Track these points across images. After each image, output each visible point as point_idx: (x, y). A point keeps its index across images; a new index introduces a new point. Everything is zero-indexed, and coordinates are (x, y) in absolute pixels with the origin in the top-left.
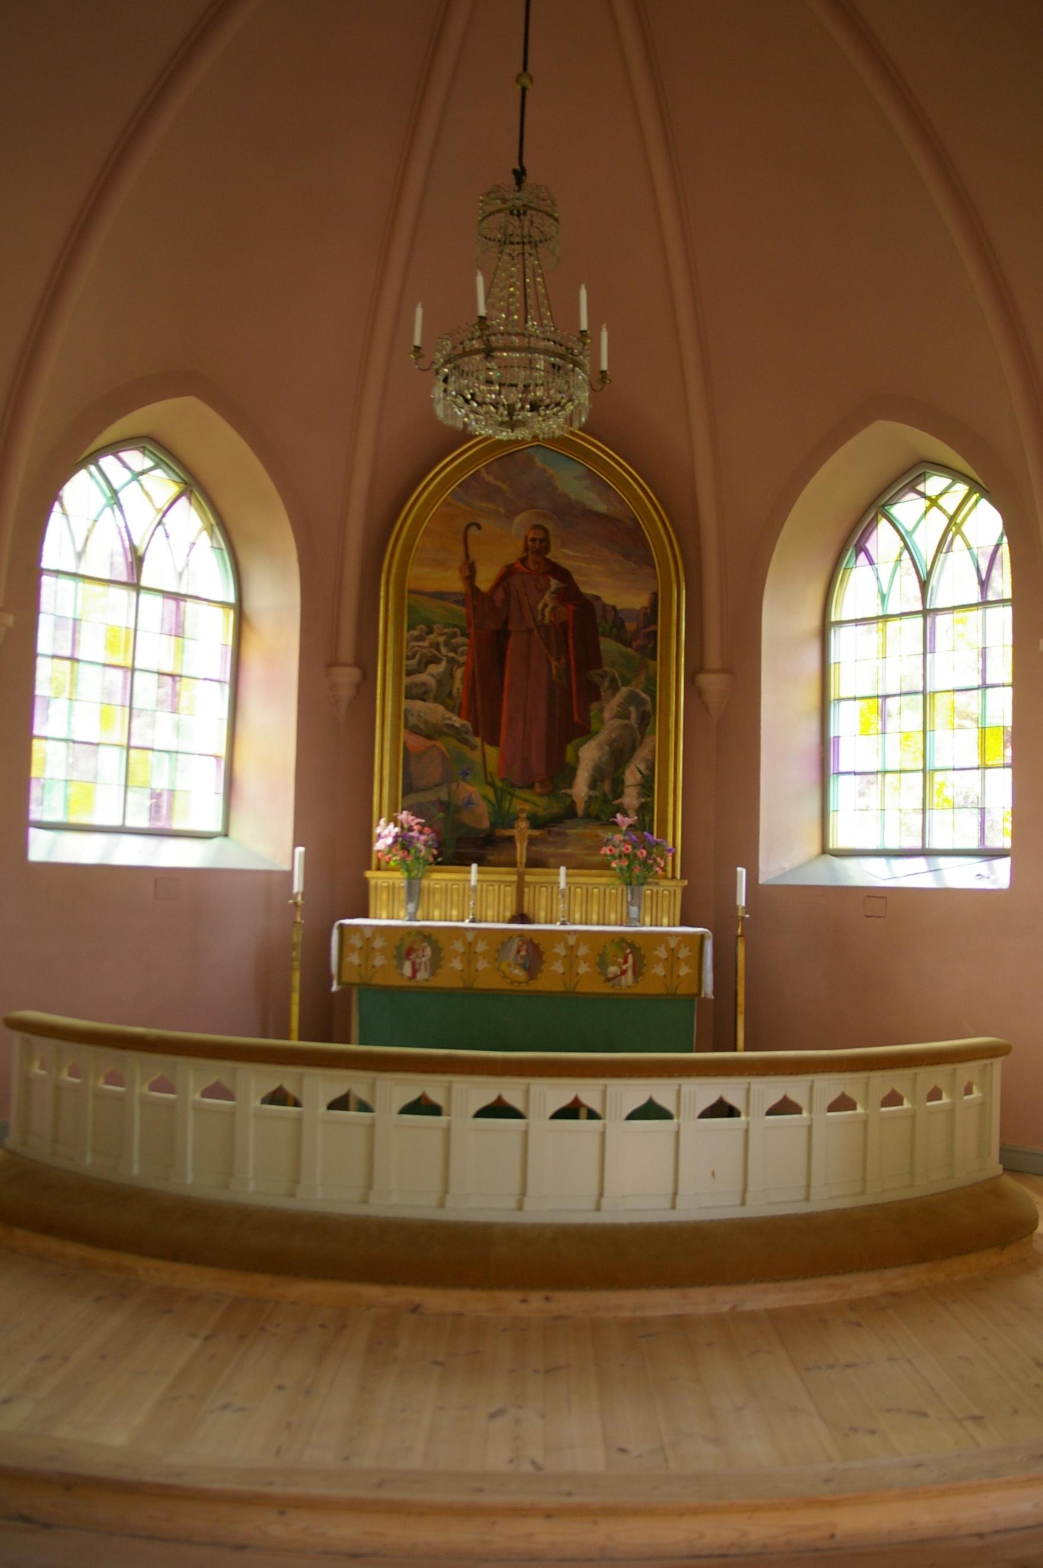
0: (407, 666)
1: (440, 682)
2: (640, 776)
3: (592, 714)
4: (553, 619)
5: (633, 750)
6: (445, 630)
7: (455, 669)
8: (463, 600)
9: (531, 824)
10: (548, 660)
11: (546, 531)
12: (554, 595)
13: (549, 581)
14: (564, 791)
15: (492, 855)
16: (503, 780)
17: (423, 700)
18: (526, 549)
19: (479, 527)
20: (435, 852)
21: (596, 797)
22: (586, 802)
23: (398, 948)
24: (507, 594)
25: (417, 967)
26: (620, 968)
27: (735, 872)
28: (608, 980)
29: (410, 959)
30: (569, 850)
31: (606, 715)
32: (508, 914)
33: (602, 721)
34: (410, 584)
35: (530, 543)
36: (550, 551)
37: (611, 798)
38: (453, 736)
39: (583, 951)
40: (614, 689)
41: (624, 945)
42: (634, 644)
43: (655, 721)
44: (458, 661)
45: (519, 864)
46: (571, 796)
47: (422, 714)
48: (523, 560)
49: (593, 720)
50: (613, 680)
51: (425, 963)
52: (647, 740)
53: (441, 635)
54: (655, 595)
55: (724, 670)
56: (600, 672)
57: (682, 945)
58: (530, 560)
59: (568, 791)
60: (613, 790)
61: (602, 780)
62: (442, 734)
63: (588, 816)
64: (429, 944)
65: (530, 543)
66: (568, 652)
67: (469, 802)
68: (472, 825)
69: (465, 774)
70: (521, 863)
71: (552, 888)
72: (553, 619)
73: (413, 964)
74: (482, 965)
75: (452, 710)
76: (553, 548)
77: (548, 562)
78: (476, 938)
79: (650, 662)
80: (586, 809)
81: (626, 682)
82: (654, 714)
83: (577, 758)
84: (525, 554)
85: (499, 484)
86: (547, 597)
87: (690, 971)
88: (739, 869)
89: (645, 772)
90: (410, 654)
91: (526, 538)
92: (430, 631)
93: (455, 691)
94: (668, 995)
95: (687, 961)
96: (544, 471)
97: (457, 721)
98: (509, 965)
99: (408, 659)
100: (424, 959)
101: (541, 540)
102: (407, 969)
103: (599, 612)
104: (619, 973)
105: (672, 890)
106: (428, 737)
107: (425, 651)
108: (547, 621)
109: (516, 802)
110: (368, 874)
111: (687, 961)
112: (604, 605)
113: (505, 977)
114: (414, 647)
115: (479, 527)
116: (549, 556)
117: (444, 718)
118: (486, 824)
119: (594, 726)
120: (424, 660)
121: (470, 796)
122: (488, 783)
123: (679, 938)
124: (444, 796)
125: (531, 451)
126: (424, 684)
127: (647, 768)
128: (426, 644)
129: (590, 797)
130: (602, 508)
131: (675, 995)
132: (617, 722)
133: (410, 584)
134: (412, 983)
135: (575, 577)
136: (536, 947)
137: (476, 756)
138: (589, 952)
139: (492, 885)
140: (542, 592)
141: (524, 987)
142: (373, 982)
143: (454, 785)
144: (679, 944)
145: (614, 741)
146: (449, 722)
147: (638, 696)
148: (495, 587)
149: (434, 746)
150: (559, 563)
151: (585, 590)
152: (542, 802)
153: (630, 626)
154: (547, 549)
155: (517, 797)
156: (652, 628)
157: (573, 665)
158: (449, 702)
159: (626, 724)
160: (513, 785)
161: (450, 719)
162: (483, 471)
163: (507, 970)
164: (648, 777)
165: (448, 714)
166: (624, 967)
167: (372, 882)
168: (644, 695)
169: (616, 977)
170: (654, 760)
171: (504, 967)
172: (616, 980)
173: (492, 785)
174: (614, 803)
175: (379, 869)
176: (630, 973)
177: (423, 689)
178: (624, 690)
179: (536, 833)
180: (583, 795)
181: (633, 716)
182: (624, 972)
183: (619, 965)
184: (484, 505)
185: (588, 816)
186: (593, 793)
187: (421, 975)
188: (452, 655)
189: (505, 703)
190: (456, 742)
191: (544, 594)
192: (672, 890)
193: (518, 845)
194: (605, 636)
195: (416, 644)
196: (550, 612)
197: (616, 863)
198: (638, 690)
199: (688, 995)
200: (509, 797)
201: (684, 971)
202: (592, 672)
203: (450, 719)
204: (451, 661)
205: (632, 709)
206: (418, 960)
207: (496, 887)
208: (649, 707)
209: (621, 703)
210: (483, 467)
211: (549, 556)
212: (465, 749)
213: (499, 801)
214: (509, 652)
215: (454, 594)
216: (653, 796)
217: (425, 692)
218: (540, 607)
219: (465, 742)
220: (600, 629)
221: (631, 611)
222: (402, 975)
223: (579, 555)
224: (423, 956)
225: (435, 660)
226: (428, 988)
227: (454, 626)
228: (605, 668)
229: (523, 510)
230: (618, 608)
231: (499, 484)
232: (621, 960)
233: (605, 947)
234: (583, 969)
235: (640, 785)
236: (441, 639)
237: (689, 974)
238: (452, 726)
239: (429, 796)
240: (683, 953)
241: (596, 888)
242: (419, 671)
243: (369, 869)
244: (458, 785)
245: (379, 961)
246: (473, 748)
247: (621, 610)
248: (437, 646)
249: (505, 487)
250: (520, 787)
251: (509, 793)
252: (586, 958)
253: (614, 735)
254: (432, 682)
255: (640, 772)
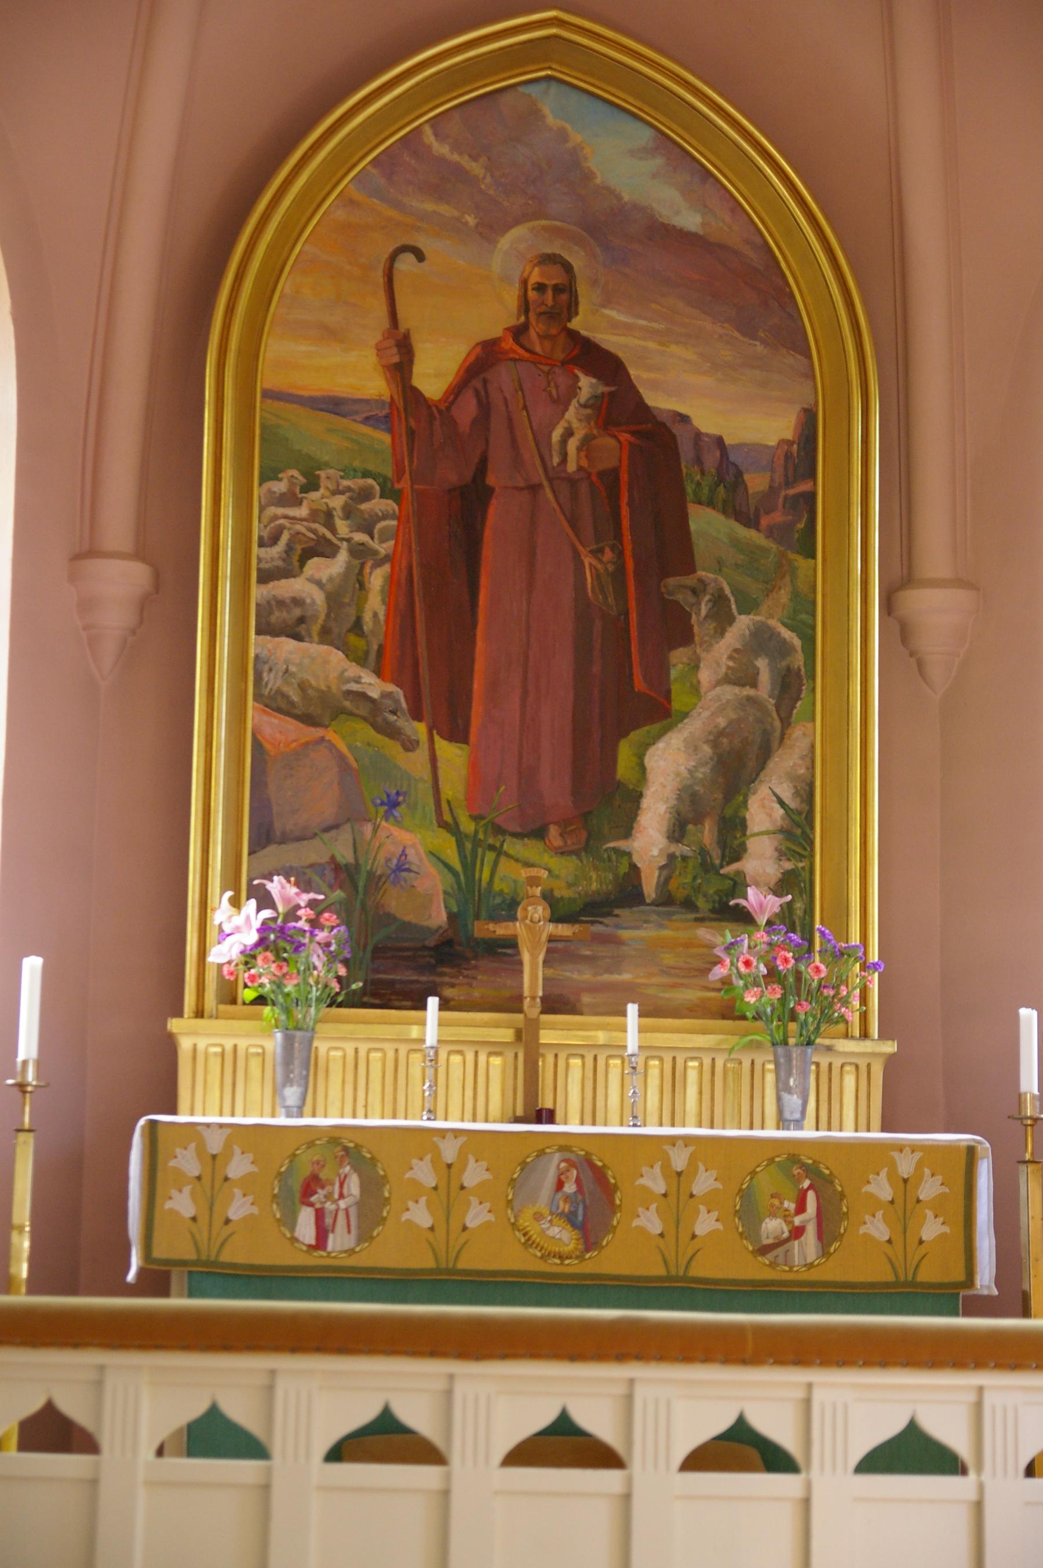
0: (260, 560)
1: (334, 600)
2: (781, 811)
3: (674, 673)
4: (584, 463)
5: (765, 754)
6: (345, 483)
7: (367, 570)
8: (386, 417)
9: (553, 913)
10: (576, 554)
11: (568, 268)
12: (589, 411)
13: (577, 379)
14: (611, 845)
15: (453, 986)
16: (476, 818)
17: (298, 637)
18: (525, 306)
19: (420, 256)
20: (342, 971)
21: (684, 858)
22: (662, 868)
23: (282, 1177)
24: (485, 408)
25: (328, 1221)
26: (788, 1222)
27: (1016, 1017)
28: (764, 1250)
29: (311, 1205)
30: (626, 977)
31: (705, 676)
32: (520, 1112)
33: (695, 689)
34: (267, 378)
35: (532, 294)
36: (577, 314)
37: (717, 862)
38: (365, 719)
39: (704, 1183)
40: (722, 618)
41: (796, 1171)
42: (764, 521)
43: (814, 690)
44: (376, 553)
45: (527, 1002)
46: (629, 855)
47: (293, 669)
48: (518, 332)
49: (675, 688)
50: (719, 600)
51: (347, 1210)
52: (797, 732)
53: (336, 492)
54: (808, 420)
55: (958, 582)
56: (690, 581)
57: (927, 1172)
58: (532, 333)
59: (621, 844)
60: (723, 843)
61: (698, 820)
62: (338, 712)
63: (666, 900)
64: (355, 1169)
65: (532, 294)
66: (619, 536)
67: (402, 867)
68: (407, 919)
69: (392, 804)
70: (533, 998)
71: (595, 1058)
72: (584, 463)
73: (320, 1215)
74: (477, 1216)
75: (361, 660)
76: (583, 306)
77: (573, 335)
78: (462, 1154)
79: (802, 563)
80: (664, 884)
81: (748, 606)
82: (813, 677)
83: (643, 769)
84: (523, 319)
85: (465, 162)
86: (571, 414)
87: (946, 1229)
88: (1024, 1012)
89: (793, 804)
90: (265, 534)
91: (524, 282)
92: (312, 485)
93: (367, 617)
94: (896, 1284)
95: (939, 1206)
96: (562, 135)
97: (373, 685)
98: (538, 1217)
99: (261, 544)
100: (342, 1204)
101: (557, 289)
102: (306, 1228)
103: (686, 450)
104: (786, 1235)
105: (863, 1063)
106: (308, 720)
107: (299, 527)
108: (571, 467)
109: (505, 867)
110: (174, 1025)
111: (939, 1206)
112: (698, 435)
113: (529, 1243)
114: (276, 517)
115: (420, 256)
116: (575, 324)
117: (342, 679)
118: (438, 917)
119: (677, 703)
120: (299, 548)
121: (404, 854)
122: (442, 824)
123: (918, 1155)
124: (345, 855)
125: (533, 90)
126: (297, 602)
127: (797, 793)
128: (303, 512)
129: (671, 857)
130: (690, 220)
131: (913, 1284)
132: (730, 693)
133: (267, 378)
134: (317, 1259)
135: (632, 372)
136: (599, 1175)
137: (416, 763)
138: (719, 1185)
139: (460, 1052)
140: (562, 403)
141: (573, 1266)
142: (227, 1256)
143: (368, 829)
144: (919, 1166)
145: (721, 733)
146: (355, 687)
147: (774, 635)
148: (456, 391)
149: (322, 739)
150: (597, 341)
151: (657, 401)
152: (566, 867)
153: (756, 482)
154: (572, 308)
155: (508, 855)
156: (804, 487)
157: (630, 566)
158: (360, 643)
159: (749, 699)
160: (498, 830)
161: (357, 680)
162: (428, 130)
163: (534, 1230)
164: (800, 813)
165: (353, 670)
166: (797, 1221)
167: (185, 1044)
168: (786, 634)
169: (780, 1243)
170: (813, 776)
171: (526, 1221)
172: (780, 1251)
173: (452, 828)
174: (722, 872)
175: (199, 1014)
176: (811, 1231)
177: (297, 612)
178: (743, 622)
179: (564, 930)
180: (655, 852)
181: (765, 677)
182: (798, 1232)
183: (787, 1218)
184: (429, 206)
185: (666, 900)
186: (680, 849)
187: (339, 1241)
188: (360, 537)
189: (480, 645)
190: (372, 732)
191: (566, 409)
192: (863, 1063)
193: (526, 957)
194: (700, 503)
195: (280, 511)
196: (579, 449)
197: (755, 995)
198: (773, 623)
199: (941, 1286)
200: (490, 856)
201: (931, 1229)
202: (672, 581)
203: (357, 680)
204: (359, 552)
205: (762, 664)
206: (329, 1206)
207: (470, 1057)
208: (798, 660)
209: (736, 650)
210: (427, 121)
211: (575, 324)
212: (393, 749)
213: (469, 865)
214: (488, 534)
215: (367, 401)
216: (812, 856)
217: (302, 620)
218: (556, 435)
219: (392, 732)
220: (689, 489)
221: (755, 449)
222: (294, 1240)
223: (642, 322)
224: (341, 1196)
225: (323, 549)
226: (353, 1269)
227: (366, 474)
228: (701, 573)
229: (517, 222)
230: (728, 441)
231: (465, 162)
232: (790, 1205)
233: (753, 1173)
234: (705, 1224)
235: (781, 831)
236: (337, 503)
237: (943, 1236)
238: (363, 696)
239: (314, 852)
240: (930, 1189)
241: (692, 1059)
242: (285, 573)
243: (179, 1013)
244: (376, 829)
245: (239, 1208)
246: (410, 746)
247: (733, 446)
248: (328, 518)
249: (476, 168)
250: (515, 835)
251: (492, 848)
252: (711, 1200)
253: (722, 722)
254: (318, 598)
255: (781, 803)
